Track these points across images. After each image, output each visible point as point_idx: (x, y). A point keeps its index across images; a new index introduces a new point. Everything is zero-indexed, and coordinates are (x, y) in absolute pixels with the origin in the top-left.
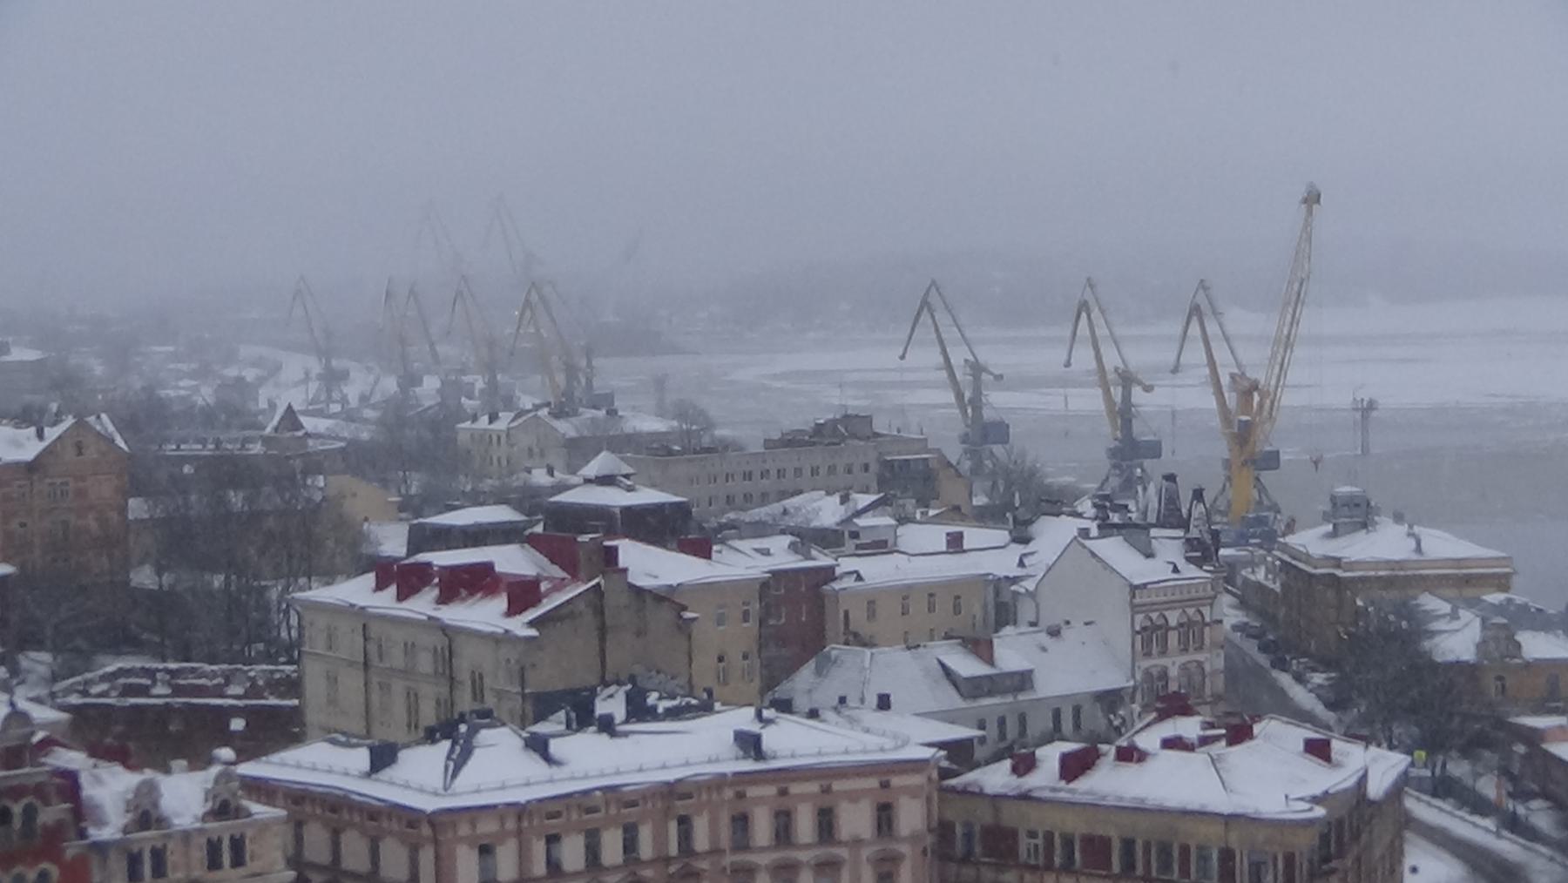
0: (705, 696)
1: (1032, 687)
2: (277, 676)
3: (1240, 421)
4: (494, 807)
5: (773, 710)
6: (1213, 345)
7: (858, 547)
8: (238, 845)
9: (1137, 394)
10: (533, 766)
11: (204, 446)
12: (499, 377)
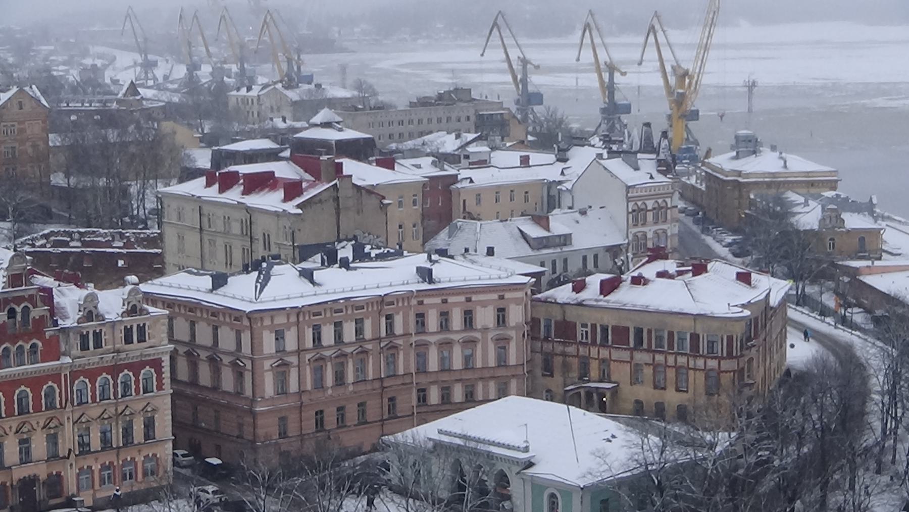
0: (398, 247)
1: (571, 244)
2: (142, 236)
3: (678, 93)
4: (284, 309)
5: (437, 256)
6: (661, 48)
7: (470, 164)
8: (141, 330)
9: (617, 77)
10: (305, 286)
11: (83, 104)
12: (246, 66)
